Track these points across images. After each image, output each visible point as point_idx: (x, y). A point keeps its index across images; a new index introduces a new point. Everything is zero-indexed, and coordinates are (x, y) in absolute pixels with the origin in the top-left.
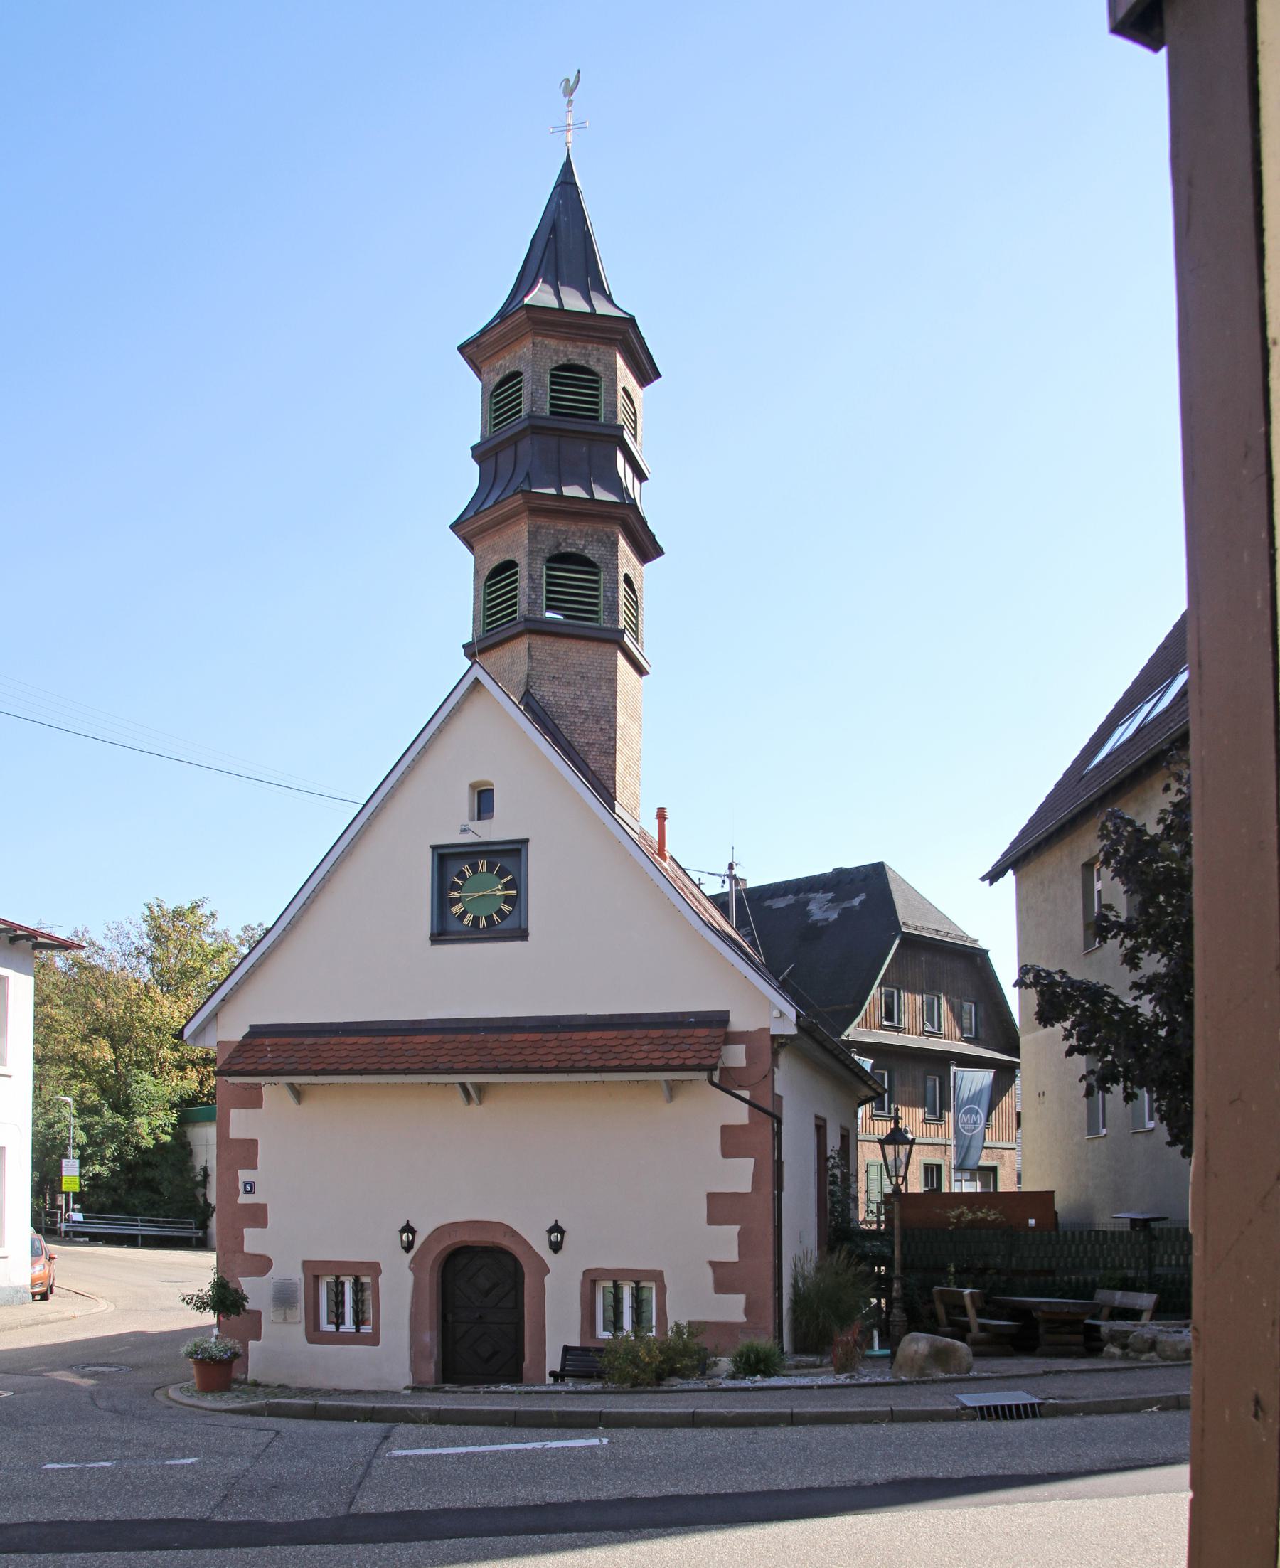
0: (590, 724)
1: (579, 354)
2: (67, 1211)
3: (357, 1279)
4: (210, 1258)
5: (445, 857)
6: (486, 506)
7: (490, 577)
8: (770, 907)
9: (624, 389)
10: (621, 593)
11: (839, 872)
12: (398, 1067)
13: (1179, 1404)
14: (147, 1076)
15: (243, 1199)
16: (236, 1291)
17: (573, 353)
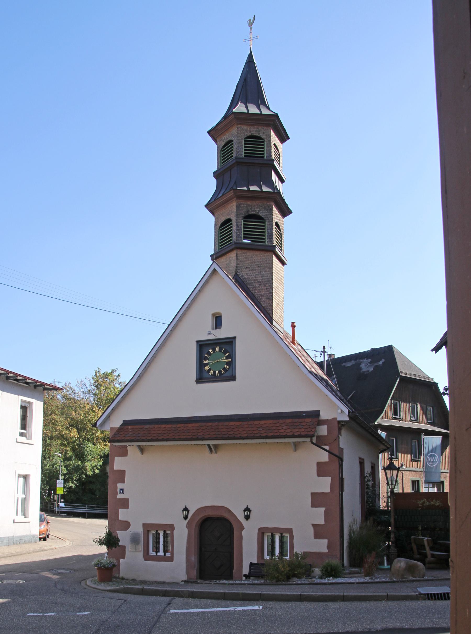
0: (262, 287)
1: (256, 131)
2: (58, 502)
3: (165, 532)
4: (105, 522)
5: (202, 346)
6: (219, 196)
7: (220, 227)
8: (345, 366)
9: (274, 145)
10: (274, 230)
11: (374, 350)
12: (182, 437)
13: (445, 597)
14: (91, 445)
15: (119, 496)
16: (115, 537)
17: (253, 131)
